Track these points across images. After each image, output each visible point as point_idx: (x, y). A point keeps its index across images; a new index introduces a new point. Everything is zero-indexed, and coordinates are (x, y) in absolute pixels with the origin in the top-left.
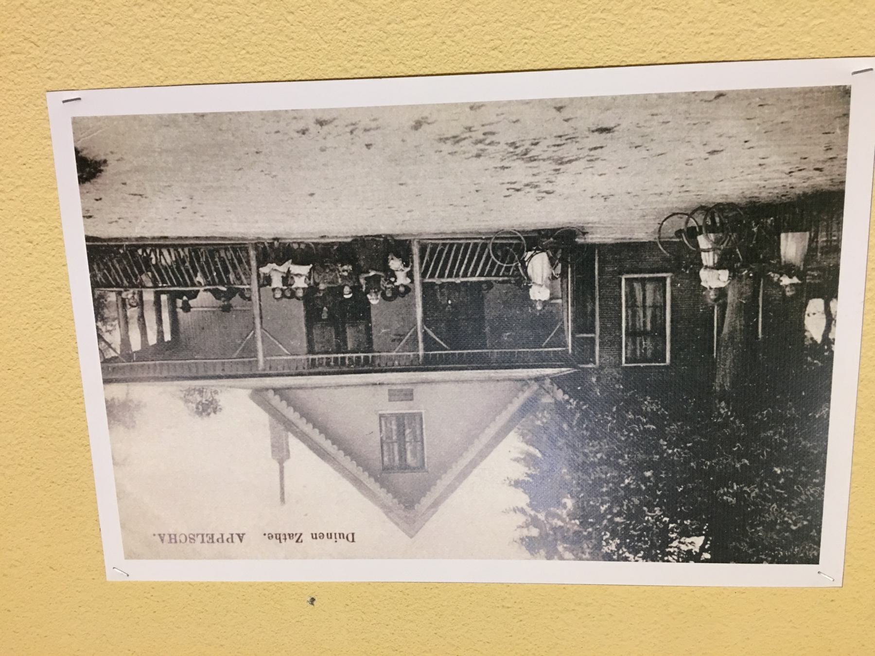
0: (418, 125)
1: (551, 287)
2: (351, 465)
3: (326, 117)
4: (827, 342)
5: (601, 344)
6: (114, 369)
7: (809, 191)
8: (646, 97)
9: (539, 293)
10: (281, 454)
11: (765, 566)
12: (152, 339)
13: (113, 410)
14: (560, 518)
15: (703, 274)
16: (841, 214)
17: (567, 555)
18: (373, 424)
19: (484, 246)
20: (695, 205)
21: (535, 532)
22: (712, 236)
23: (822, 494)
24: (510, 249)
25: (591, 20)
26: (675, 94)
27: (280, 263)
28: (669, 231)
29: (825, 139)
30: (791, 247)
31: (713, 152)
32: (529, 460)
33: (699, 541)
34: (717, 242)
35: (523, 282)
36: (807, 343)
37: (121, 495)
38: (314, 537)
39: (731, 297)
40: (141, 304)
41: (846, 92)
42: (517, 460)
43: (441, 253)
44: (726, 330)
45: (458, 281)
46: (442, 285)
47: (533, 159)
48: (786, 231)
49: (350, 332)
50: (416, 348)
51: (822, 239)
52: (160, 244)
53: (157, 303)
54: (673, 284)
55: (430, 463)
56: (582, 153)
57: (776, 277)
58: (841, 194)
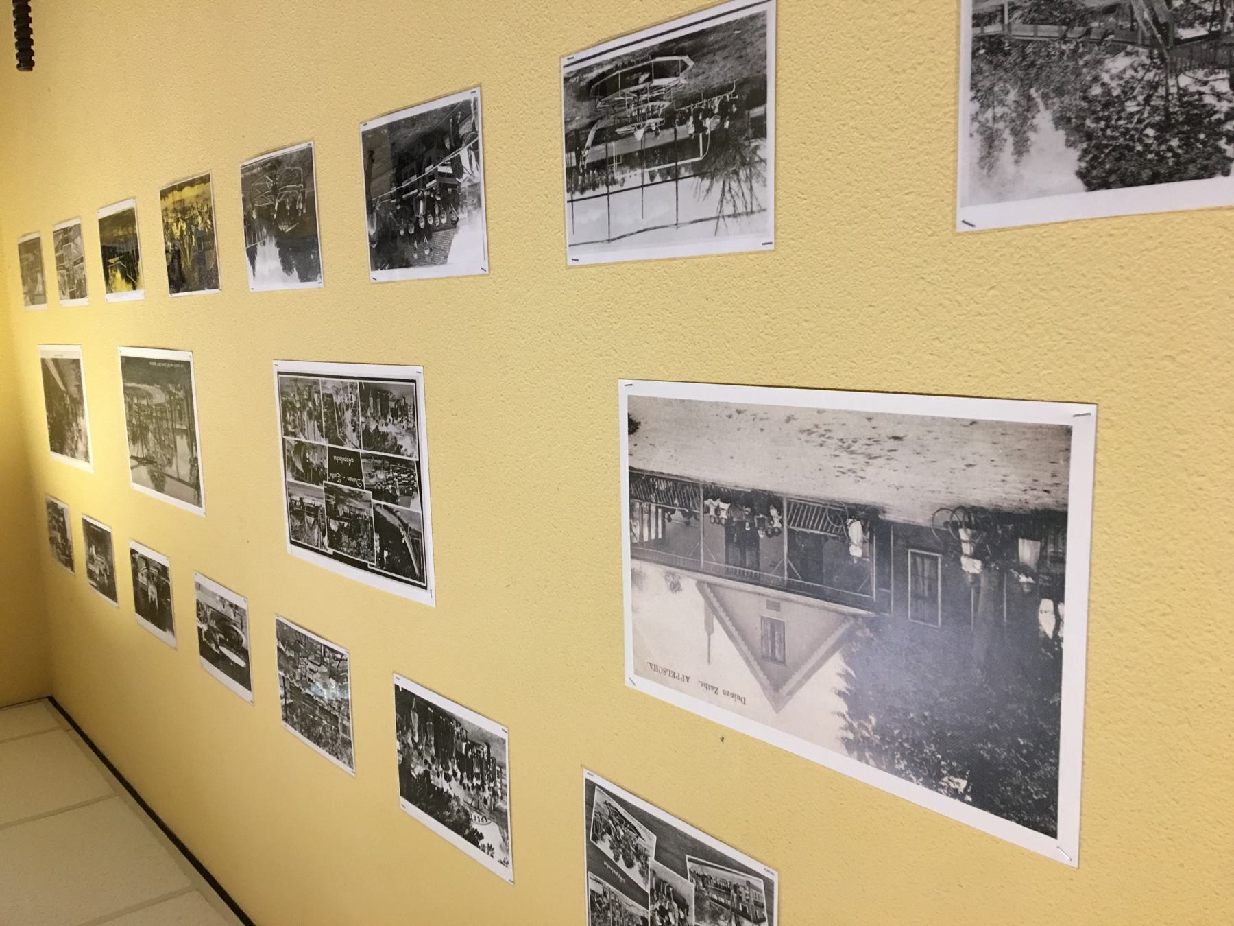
0: (789, 420)
1: (863, 548)
2: (745, 648)
3: (741, 409)
4: (1057, 639)
5: (895, 600)
6: (638, 551)
7: (1040, 508)
8: (923, 418)
9: (856, 551)
10: (710, 630)
11: (1013, 824)
12: (653, 537)
13: (636, 576)
14: (867, 729)
15: (964, 560)
16: (1065, 531)
17: (871, 761)
18: (757, 623)
19: (824, 509)
20: (957, 505)
21: (851, 736)
22: (969, 530)
23: (1057, 774)
24: (842, 513)
25: (893, 359)
26: (943, 419)
27: (715, 500)
28: (940, 523)
29: (1051, 467)
30: (1027, 551)
31: (969, 466)
32: (846, 676)
33: (964, 783)
34: (973, 536)
35: (845, 541)
36: (1041, 636)
37: (635, 632)
38: (724, 693)
39: (983, 582)
40: (649, 512)
41: (1068, 431)
42: (840, 675)
43: (800, 509)
44: (980, 610)
45: (809, 531)
46: (799, 533)
47: (852, 452)
48: (1023, 538)
49: (748, 553)
50: (782, 575)
51: (1050, 549)
52: (661, 477)
53: (657, 512)
54: (943, 564)
55: (789, 661)
56: (883, 453)
57: (1016, 574)
58: (1064, 515)
